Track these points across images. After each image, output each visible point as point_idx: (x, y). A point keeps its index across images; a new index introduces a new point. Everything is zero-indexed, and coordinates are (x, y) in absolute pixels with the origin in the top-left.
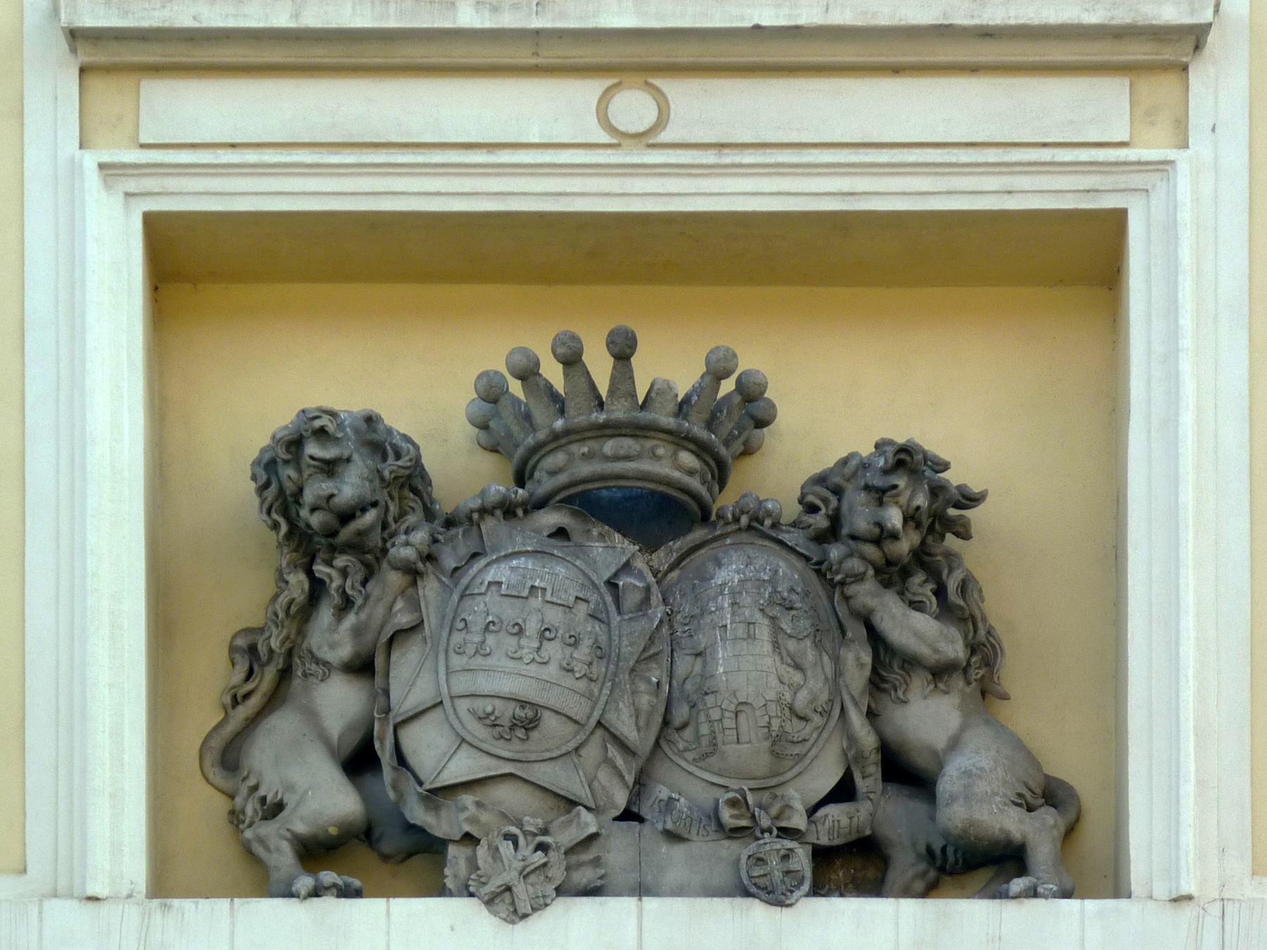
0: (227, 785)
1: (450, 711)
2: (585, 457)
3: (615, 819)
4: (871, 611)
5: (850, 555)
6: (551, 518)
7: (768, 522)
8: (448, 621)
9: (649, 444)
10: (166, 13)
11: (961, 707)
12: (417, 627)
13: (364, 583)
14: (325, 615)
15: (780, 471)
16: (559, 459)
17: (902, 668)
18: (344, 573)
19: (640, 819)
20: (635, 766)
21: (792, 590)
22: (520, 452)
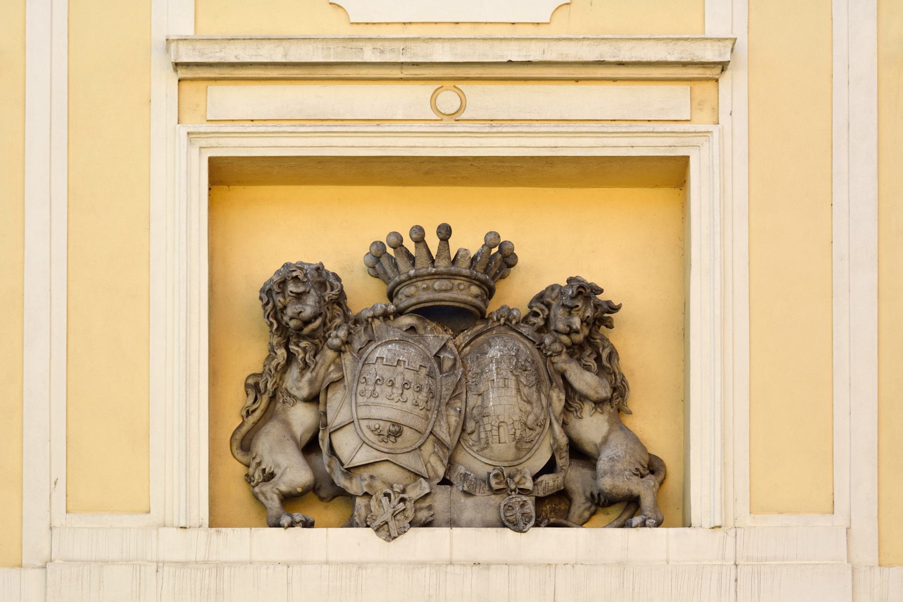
0: (245, 459)
1: (357, 426)
4: (565, 371)
5: (554, 341)
6: (407, 321)
8: (357, 377)
9: (456, 282)
10: (222, 54)
11: (608, 421)
13: (314, 356)
14: (294, 371)
15: (517, 292)
16: (412, 290)
17: (580, 400)
18: (305, 350)
19: (450, 484)
20: (448, 454)
21: (526, 360)
22: (392, 284)
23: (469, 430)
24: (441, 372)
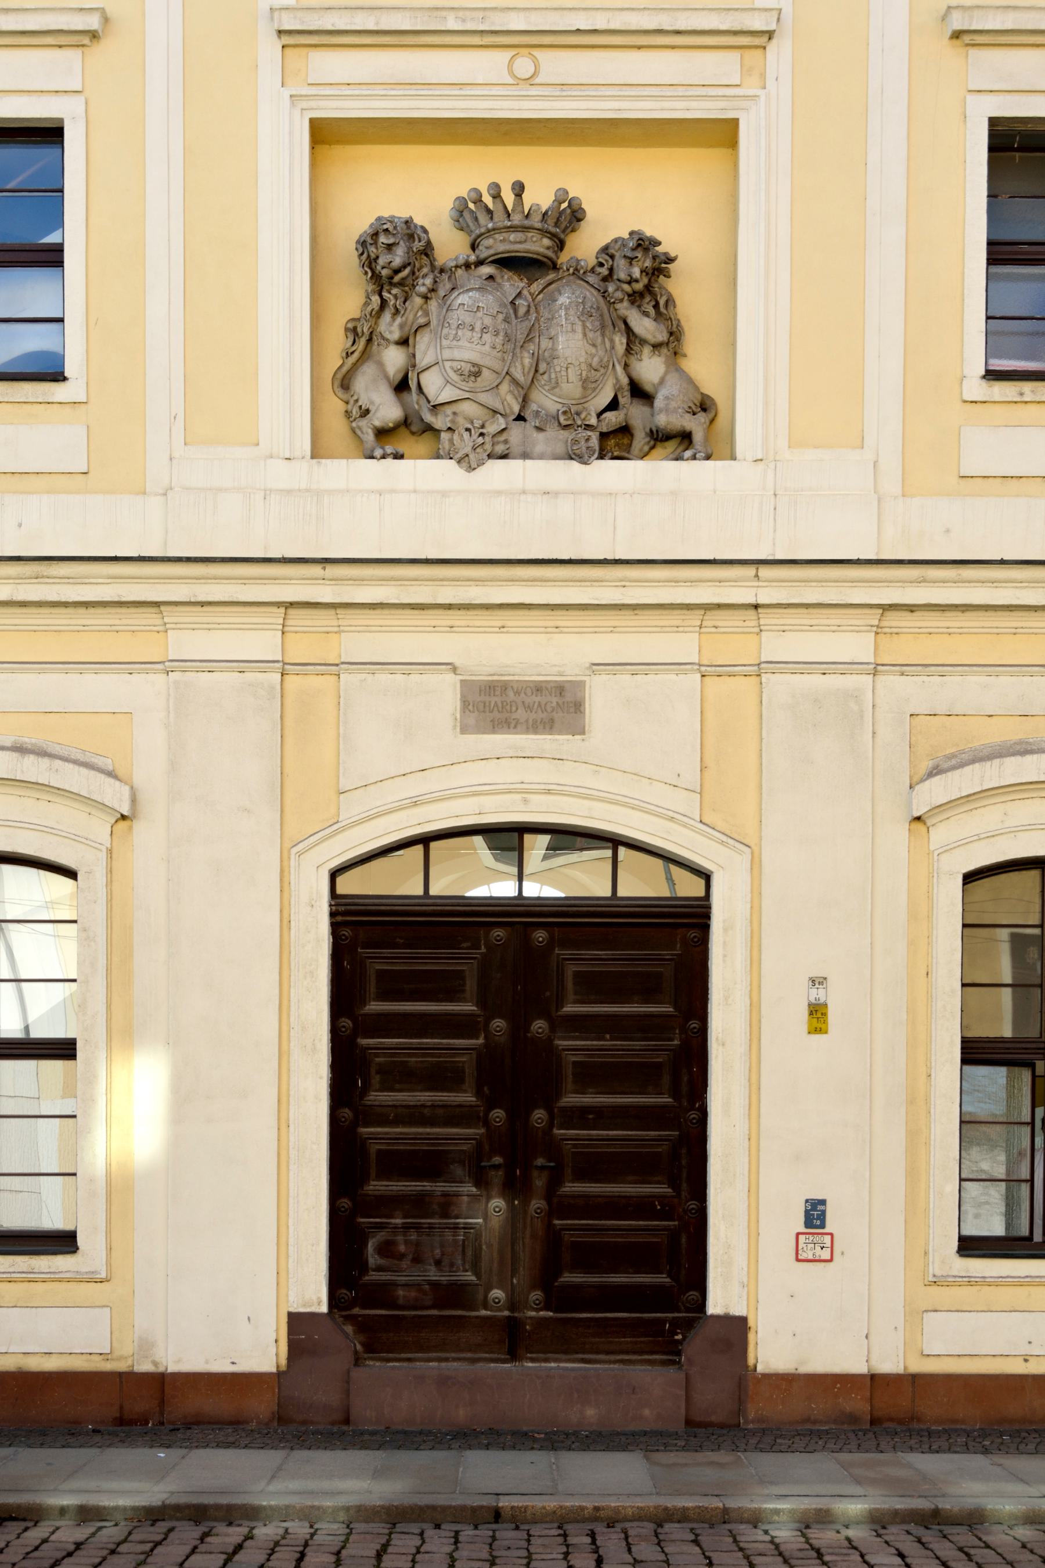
2: (503, 241)
3: (514, 420)
5: (617, 290)
6: (486, 270)
7: (582, 272)
12: (427, 324)
13: (404, 303)
14: (387, 316)
18: (396, 297)
20: (522, 393)
23: (541, 371)
24: (516, 317)
